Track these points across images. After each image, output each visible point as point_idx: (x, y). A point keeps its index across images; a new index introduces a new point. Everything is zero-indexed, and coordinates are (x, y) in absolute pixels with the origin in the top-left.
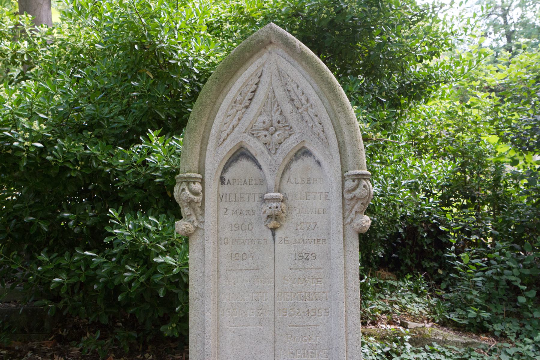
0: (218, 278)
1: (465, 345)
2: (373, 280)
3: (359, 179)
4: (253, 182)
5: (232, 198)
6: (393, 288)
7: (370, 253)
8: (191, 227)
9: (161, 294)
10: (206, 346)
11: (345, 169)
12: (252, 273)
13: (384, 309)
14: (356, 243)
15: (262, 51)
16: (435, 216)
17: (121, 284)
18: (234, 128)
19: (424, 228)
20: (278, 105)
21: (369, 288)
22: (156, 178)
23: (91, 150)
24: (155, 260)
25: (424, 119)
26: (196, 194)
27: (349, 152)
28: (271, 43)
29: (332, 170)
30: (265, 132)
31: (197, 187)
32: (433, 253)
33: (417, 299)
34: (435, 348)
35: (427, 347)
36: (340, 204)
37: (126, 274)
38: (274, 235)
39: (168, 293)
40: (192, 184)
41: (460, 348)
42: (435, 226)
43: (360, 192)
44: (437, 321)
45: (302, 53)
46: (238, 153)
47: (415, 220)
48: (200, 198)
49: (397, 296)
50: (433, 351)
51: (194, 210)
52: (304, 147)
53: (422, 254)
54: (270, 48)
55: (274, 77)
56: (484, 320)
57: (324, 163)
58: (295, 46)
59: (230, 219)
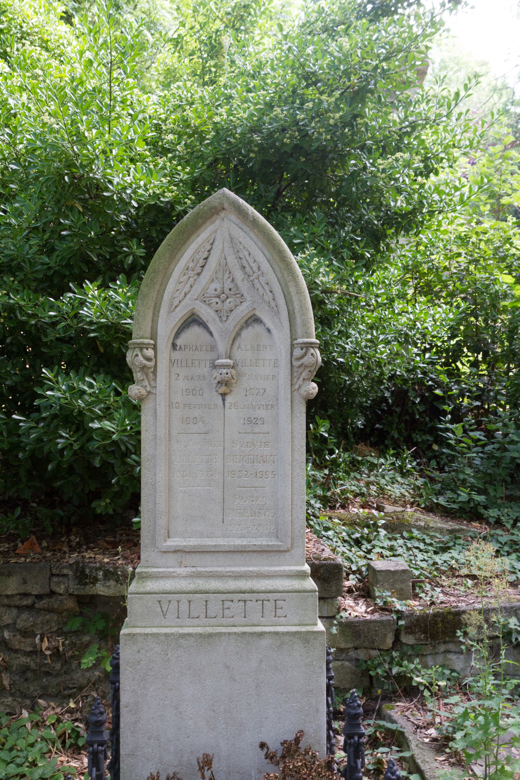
0: (170, 440)
1: (451, 532)
2: (346, 455)
3: (307, 347)
4: (204, 349)
5: (184, 364)
6: (372, 467)
7: (346, 423)
8: (144, 392)
9: (97, 463)
10: (158, 506)
11: (294, 337)
12: (203, 436)
13: (358, 491)
14: (304, 409)
15: (215, 216)
16: (431, 376)
17: (51, 452)
18: (186, 294)
19: (416, 391)
20: (230, 273)
21: (340, 464)
22: (89, 333)
23: (15, 299)
24: (90, 425)
25: (426, 247)
26: (149, 359)
27: (298, 321)
28: (224, 209)
29: (281, 338)
30: (217, 300)
31: (150, 353)
32: (426, 423)
33: (399, 479)
34: (414, 535)
35: (405, 534)
36: (288, 371)
37: (59, 440)
38: (224, 400)
39: (105, 463)
40: (145, 350)
41: (444, 536)
42: (430, 389)
43: (307, 360)
44: (423, 506)
45: (255, 222)
46: (190, 320)
47: (405, 381)
48: (152, 364)
49: (376, 476)
50: (411, 538)
51: (147, 375)
52: (254, 315)
53: (413, 425)
54: (222, 214)
55: (226, 244)
56: (479, 504)
57: (274, 331)
58: (247, 214)
59: (181, 384)
